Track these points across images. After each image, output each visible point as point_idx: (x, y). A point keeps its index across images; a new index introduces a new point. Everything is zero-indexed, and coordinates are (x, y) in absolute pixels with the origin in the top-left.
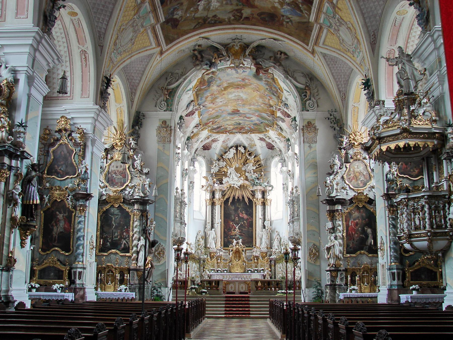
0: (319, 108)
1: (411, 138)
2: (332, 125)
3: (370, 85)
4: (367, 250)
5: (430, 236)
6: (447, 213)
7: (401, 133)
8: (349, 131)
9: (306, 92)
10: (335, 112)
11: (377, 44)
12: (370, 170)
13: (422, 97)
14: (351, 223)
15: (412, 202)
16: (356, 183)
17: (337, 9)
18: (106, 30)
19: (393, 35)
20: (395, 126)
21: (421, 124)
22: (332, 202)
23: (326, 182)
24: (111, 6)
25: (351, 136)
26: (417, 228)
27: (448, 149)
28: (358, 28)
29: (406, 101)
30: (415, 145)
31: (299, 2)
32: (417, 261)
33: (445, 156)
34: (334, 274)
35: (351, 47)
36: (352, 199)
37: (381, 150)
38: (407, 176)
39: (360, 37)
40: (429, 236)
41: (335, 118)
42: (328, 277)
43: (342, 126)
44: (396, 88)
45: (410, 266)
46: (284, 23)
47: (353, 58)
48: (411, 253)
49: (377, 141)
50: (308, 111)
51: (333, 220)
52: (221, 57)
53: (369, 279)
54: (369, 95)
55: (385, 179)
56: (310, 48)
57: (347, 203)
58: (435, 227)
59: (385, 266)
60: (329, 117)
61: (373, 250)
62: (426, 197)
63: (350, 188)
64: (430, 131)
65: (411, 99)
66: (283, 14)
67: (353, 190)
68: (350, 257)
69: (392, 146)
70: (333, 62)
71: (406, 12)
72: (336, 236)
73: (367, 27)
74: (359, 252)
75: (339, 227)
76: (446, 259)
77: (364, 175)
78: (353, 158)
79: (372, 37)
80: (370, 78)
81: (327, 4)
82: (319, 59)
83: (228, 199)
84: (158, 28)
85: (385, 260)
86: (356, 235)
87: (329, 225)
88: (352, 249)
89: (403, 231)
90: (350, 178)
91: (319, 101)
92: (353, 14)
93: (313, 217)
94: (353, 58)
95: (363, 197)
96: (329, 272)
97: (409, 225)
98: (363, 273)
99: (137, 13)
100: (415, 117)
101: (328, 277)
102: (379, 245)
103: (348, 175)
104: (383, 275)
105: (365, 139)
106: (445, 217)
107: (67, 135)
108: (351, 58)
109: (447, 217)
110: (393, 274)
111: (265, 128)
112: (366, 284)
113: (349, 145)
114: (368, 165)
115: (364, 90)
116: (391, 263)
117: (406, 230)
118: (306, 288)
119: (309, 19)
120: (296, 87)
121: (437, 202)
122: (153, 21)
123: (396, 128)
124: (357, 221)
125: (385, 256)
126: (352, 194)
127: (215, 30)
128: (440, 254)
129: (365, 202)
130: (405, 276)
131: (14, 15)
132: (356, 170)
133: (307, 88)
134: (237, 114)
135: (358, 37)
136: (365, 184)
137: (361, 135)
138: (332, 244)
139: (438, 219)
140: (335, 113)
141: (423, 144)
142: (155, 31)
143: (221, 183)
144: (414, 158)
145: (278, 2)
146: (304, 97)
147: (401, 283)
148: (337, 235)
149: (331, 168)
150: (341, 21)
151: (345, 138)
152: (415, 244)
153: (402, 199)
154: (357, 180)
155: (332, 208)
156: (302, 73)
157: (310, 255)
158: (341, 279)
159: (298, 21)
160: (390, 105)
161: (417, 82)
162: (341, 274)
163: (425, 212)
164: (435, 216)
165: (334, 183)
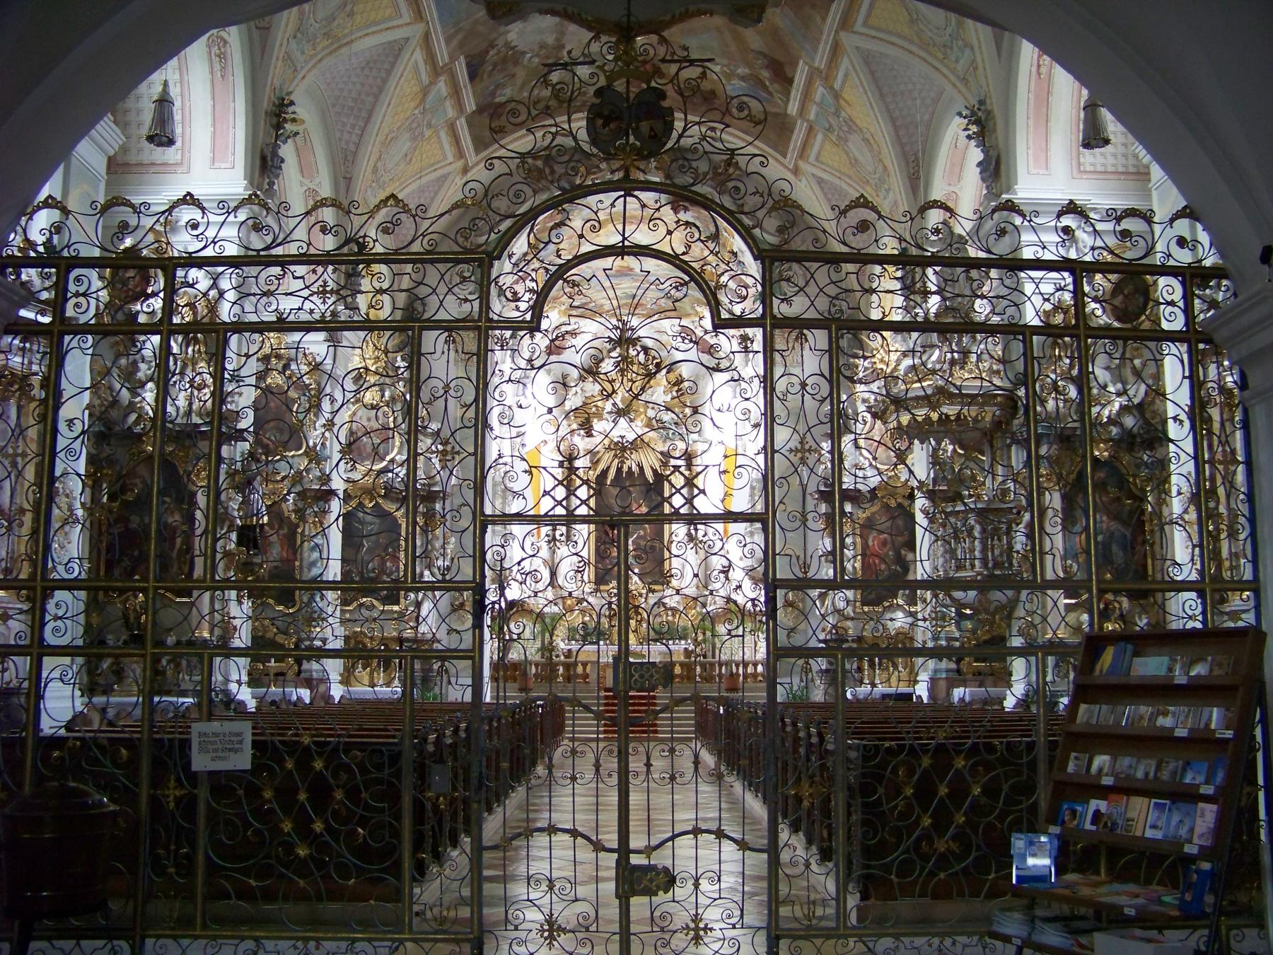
18: (358, 146)
19: (953, 165)
24: (371, 99)
26: (959, 567)
39: (888, 162)
52: (594, 173)
56: (790, 160)
58: (990, 565)
73: (902, 146)
79: (912, 165)
81: (821, 89)
83: (604, 473)
84: (462, 124)
97: (946, 561)
99: (420, 104)
107: (280, 367)
111: (693, 308)
122: (451, 113)
126: (874, 481)
131: (208, 163)
134: (627, 275)
139: (997, 552)
142: (454, 131)
143: (589, 434)
164: (993, 546)
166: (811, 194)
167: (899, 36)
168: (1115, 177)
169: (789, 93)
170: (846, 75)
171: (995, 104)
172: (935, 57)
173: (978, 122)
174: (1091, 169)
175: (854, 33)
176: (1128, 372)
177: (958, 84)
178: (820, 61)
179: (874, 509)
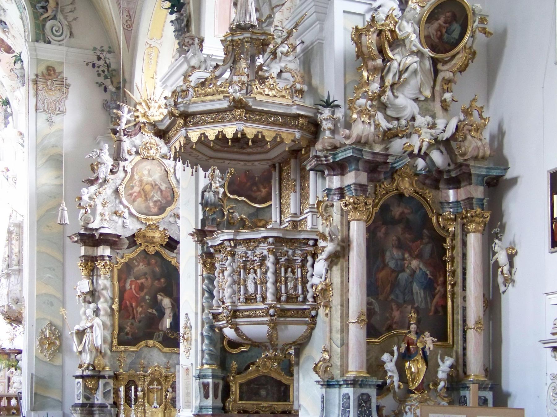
0: (72, 40)
1: (250, 120)
2: (101, 79)
4: (161, 339)
5: (274, 315)
6: (309, 274)
7: (230, 109)
8: (136, 96)
10: (109, 52)
13: (279, 41)
14: (131, 285)
15: (244, 249)
16: (143, 206)
20: (219, 93)
21: (272, 97)
22: (90, 239)
23: (80, 199)
25: (138, 107)
26: (248, 299)
27: (320, 151)
29: (247, 45)
30: (256, 136)
32: (253, 364)
33: (313, 163)
34: (90, 384)
36: (134, 236)
37: (187, 138)
38: (244, 199)
40: (271, 316)
41: (108, 67)
42: (78, 389)
45: (239, 372)
48: (243, 349)
50: (49, 42)
51: (93, 276)
53: (161, 394)
54: (180, 24)
55: (200, 201)
57: (123, 244)
58: (283, 298)
59: (190, 371)
60: (96, 62)
61: (172, 341)
62: (270, 240)
63: (131, 214)
65: (258, 43)
69: (212, 133)
72: (98, 309)
74: (143, 343)
75: (104, 292)
76: (302, 360)
77: (161, 191)
78: (140, 154)
85: (192, 360)
86: (140, 309)
87: (85, 285)
88: (130, 337)
89: (223, 302)
90: (131, 194)
91: (73, 24)
93: (51, 266)
96: (80, 380)
98: (151, 383)
100: (262, 80)
101: (78, 389)
102: (182, 330)
103: (129, 187)
104: (187, 388)
105: (158, 114)
106: (305, 282)
109: (308, 281)
110: (205, 386)
112: (155, 404)
113: (135, 125)
114: (172, 170)
115: (171, 13)
116: (203, 365)
117: (228, 303)
118: (31, 410)
121: (290, 252)
123: (221, 97)
124: (143, 280)
125: (192, 352)
126: (133, 227)
127: (309, 32)
128: (292, 351)
130: (229, 390)
132: (146, 179)
136: (162, 210)
138: (89, 324)
139: (290, 285)
140: (108, 55)
144: (256, 163)
146: (41, 11)
147: (219, 404)
149: (93, 170)
152: (245, 329)
153: (223, 241)
154: (146, 200)
155: (91, 251)
157: (41, 344)
160: (214, 47)
161: (272, 9)
162: (105, 385)
164: (286, 278)
165: (99, 201)
176: (437, 107)
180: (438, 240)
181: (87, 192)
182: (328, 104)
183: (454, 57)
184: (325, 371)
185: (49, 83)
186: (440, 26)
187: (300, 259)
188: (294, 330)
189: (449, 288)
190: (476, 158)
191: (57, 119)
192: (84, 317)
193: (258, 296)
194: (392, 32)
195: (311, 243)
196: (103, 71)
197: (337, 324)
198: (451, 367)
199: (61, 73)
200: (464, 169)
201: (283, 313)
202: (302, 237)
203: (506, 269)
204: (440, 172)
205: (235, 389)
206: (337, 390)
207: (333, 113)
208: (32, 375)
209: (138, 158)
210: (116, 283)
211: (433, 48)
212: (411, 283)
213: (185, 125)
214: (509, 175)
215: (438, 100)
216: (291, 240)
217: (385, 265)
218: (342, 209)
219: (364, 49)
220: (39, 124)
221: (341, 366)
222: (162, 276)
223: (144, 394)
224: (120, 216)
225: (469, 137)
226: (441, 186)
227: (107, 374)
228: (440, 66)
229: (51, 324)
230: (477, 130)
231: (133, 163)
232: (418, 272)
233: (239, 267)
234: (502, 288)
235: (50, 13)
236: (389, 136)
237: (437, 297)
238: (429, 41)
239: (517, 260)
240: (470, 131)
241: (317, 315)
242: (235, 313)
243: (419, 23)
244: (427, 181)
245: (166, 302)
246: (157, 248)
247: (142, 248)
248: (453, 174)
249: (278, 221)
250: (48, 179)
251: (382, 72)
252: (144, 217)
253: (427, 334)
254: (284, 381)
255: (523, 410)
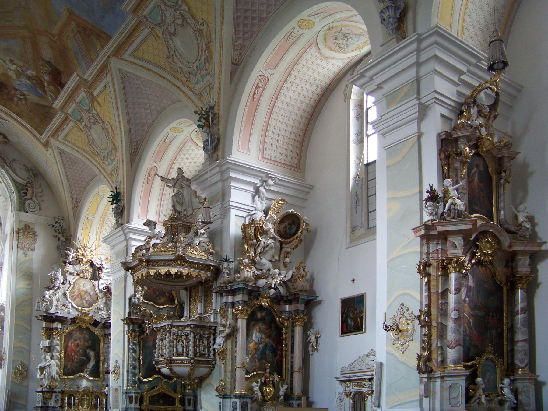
0: (41, 211)
1: (184, 266)
2: (57, 234)
3: (120, 200)
4: (88, 373)
7: (174, 260)
8: (78, 245)
9: (27, 190)
10: (63, 220)
11: (138, 157)
12: (98, 291)
17: (96, 104)
19: (159, 151)
21: (196, 254)
22: (50, 318)
23: (44, 297)
25: (79, 250)
26: (178, 355)
28: (119, 132)
30: (188, 274)
31: (45, 80)
32: (157, 387)
34: (47, 396)
35: (103, 151)
36: (74, 318)
37: (148, 273)
41: (62, 228)
42: (39, 398)
43: (69, 238)
44: (170, 211)
46: (15, 99)
47: (102, 164)
49: (145, 264)
50: (27, 212)
53: (89, 402)
56: (44, 138)
57: (68, 322)
58: (198, 355)
60: (54, 224)
62: (192, 326)
63: (72, 306)
64: (205, 263)
66: (17, 87)
67: (76, 309)
68: (67, 378)
69: (163, 271)
70: (72, 162)
71: (181, 130)
73: (131, 134)
74: (78, 375)
75: (57, 347)
77: (90, 295)
80: (121, 192)
81: (83, 93)
82: (52, 154)
86: (76, 357)
88: (70, 371)
90: (73, 296)
92: (116, 114)
94: (102, 164)
95: (87, 318)
96: (41, 394)
98: (83, 396)
101: (39, 398)
103: (72, 292)
106: (209, 347)
108: (99, 164)
110: (131, 398)
112: (85, 407)
113: (76, 260)
115: (112, 204)
116: (128, 386)
119: (53, 104)
120: (14, 181)
121: (202, 332)
124: (78, 342)
126: (74, 313)
129: (90, 324)
133: (28, 185)
135: (116, 143)
136: (90, 305)
137: (91, 251)
138: (48, 364)
139: (202, 348)
140: (62, 221)
141: (197, 274)
145: (14, 71)
146: (23, 195)
148: (54, 354)
149: (52, 282)
150: (97, 118)
151: (72, 251)
152: (175, 369)
153: (165, 325)
154: (82, 299)
156: (24, 166)
157: (15, 373)
158: (56, 401)
159: (36, 102)
162: (56, 396)
163: (190, 340)
164: (200, 345)
165: (54, 299)
166: (53, 160)
167: (155, 65)
168: (280, 165)
169: (59, 93)
170: (106, 86)
171: (221, 110)
172: (179, 80)
173: (207, 119)
174: (269, 158)
175: (121, 59)
176: (281, 265)
177: (193, 98)
178: (89, 75)
179: (72, 328)
180: (279, 329)
181: (48, 294)
182: (226, 261)
183: (291, 241)
184: (222, 391)
185: (26, 233)
186: (286, 226)
187: (207, 336)
188: (202, 371)
189: (284, 352)
190: (301, 291)
191: (30, 253)
192: (44, 360)
193: (185, 353)
194: (262, 227)
195: (213, 328)
196: (58, 230)
197: (229, 368)
198: (286, 389)
199: (33, 229)
200: (297, 296)
201: (198, 362)
202: (209, 325)
203: (314, 344)
204: (282, 297)
205: (146, 399)
206: (229, 400)
207: (228, 265)
208: (9, 391)
209: (78, 277)
210: (63, 343)
211: (281, 236)
212: (265, 349)
213: (147, 266)
214: (318, 299)
215: (282, 262)
216: (202, 326)
217: (253, 340)
218: (233, 312)
219: (247, 235)
220: (19, 255)
221: (231, 388)
222: (90, 340)
223: (79, 402)
224: (66, 307)
225: (298, 280)
226: (281, 303)
227: (57, 391)
228: (284, 245)
229: (22, 363)
230: (303, 277)
231: (75, 280)
232: (269, 344)
233: (173, 339)
234: (311, 353)
235: (28, 196)
236: (258, 277)
237: (278, 356)
238: (279, 232)
239: (320, 340)
240: (299, 278)
241: (215, 363)
242: (171, 361)
243: (274, 224)
244: (274, 301)
245: (92, 353)
246: (88, 326)
247: (79, 324)
248: (289, 298)
249: (188, 316)
250: (23, 285)
251: (255, 247)
252: (80, 308)
253: (275, 374)
254: (172, 395)
255: (328, 409)
